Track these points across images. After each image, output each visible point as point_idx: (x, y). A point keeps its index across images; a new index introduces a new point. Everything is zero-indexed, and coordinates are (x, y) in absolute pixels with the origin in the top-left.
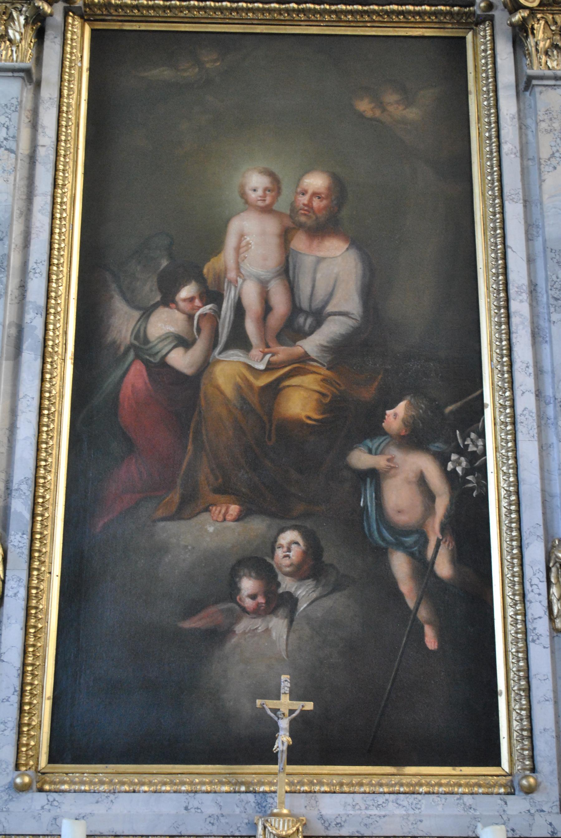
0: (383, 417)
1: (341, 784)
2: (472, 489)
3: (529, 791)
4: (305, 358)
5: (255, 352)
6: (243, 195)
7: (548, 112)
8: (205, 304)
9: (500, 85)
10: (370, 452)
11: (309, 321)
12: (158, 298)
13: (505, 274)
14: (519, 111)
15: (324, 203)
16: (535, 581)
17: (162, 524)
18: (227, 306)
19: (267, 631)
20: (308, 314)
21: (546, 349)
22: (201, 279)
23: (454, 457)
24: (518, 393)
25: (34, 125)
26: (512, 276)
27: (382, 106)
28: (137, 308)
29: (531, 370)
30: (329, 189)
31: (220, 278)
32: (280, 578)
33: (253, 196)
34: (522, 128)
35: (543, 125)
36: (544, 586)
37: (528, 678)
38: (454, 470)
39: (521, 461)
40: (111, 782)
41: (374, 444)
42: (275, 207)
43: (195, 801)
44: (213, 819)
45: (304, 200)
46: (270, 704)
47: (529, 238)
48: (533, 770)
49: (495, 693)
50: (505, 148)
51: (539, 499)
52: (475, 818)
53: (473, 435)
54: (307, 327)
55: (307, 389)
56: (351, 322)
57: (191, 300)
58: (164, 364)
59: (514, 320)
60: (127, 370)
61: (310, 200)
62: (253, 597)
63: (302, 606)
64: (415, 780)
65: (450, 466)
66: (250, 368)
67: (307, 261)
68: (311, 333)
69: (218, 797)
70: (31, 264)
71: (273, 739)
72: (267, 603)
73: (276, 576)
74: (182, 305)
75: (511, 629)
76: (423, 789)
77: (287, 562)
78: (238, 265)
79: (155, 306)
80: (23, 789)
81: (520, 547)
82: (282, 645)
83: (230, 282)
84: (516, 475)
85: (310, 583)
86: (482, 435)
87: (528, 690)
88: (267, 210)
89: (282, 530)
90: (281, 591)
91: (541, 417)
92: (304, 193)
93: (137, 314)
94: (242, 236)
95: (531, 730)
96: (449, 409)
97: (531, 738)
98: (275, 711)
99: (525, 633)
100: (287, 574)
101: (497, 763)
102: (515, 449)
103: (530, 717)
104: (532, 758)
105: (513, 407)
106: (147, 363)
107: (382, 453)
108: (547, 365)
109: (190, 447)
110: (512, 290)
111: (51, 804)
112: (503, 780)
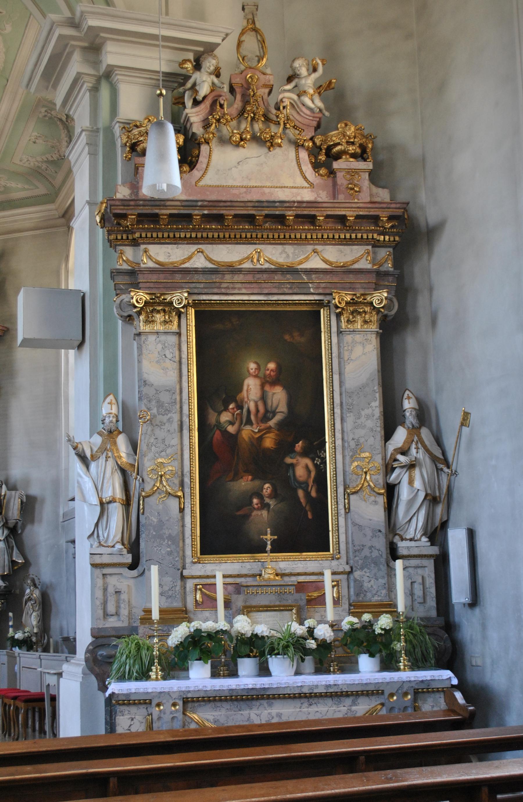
0: (295, 446)
1: (285, 559)
2: (322, 469)
3: (338, 559)
4: (270, 427)
5: (254, 426)
6: (248, 371)
7: (347, 343)
8: (238, 410)
9: (332, 332)
10: (291, 458)
11: (271, 415)
12: (223, 408)
13: (333, 399)
14: (338, 340)
15: (274, 373)
16: (341, 498)
17: (228, 483)
18: (245, 410)
19: (262, 514)
20: (271, 412)
21: (345, 424)
22: (236, 402)
23: (317, 459)
24: (336, 439)
25: (180, 350)
26: (335, 400)
27: (292, 337)
28: (217, 412)
29: (340, 432)
30: (276, 368)
31: (242, 401)
32: (265, 498)
33: (251, 371)
34: (339, 347)
35: (346, 348)
36: (343, 500)
37: (338, 527)
38: (317, 463)
39: (337, 461)
40: (219, 560)
41: (292, 455)
42: (259, 375)
43: (244, 565)
44: (249, 570)
45: (268, 372)
46: (265, 537)
47: (341, 387)
48: (339, 553)
49: (328, 531)
50: (334, 355)
51: (342, 473)
52: (323, 567)
53: (323, 452)
54: (270, 417)
55: (270, 438)
56: (283, 415)
57: (233, 409)
58: (226, 431)
59: (336, 415)
60: (214, 434)
61: (270, 372)
62: (257, 504)
63: (272, 507)
64: (305, 557)
65: (315, 462)
66: (253, 431)
67: (270, 394)
68: (272, 419)
69: (251, 563)
70: (183, 400)
71: (266, 547)
72: (261, 506)
73: (263, 498)
74: (230, 410)
75: (334, 512)
76: (308, 559)
77: (267, 493)
78: (247, 395)
79: (222, 411)
80: (195, 563)
81: (336, 488)
82: (266, 519)
83: (245, 402)
84: (336, 465)
85: (274, 500)
86: (325, 451)
87: (338, 530)
88: (256, 376)
89: (265, 484)
90: (265, 502)
91: (343, 446)
92: (268, 370)
93: (216, 414)
94: (248, 386)
95: (339, 542)
96: (316, 443)
97: (339, 544)
98: (266, 539)
99: (338, 513)
100: (267, 497)
101: (329, 551)
102: (335, 457)
103: (338, 538)
104: (339, 549)
105: (335, 443)
106: (220, 430)
107: (295, 458)
108: (345, 430)
109: (236, 458)
110: (335, 405)
111: (203, 566)
112: (331, 556)
